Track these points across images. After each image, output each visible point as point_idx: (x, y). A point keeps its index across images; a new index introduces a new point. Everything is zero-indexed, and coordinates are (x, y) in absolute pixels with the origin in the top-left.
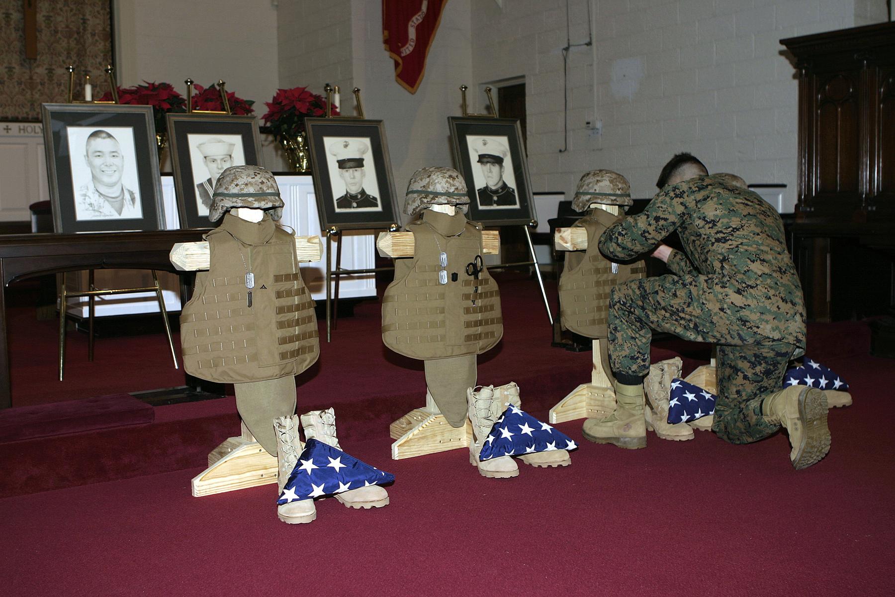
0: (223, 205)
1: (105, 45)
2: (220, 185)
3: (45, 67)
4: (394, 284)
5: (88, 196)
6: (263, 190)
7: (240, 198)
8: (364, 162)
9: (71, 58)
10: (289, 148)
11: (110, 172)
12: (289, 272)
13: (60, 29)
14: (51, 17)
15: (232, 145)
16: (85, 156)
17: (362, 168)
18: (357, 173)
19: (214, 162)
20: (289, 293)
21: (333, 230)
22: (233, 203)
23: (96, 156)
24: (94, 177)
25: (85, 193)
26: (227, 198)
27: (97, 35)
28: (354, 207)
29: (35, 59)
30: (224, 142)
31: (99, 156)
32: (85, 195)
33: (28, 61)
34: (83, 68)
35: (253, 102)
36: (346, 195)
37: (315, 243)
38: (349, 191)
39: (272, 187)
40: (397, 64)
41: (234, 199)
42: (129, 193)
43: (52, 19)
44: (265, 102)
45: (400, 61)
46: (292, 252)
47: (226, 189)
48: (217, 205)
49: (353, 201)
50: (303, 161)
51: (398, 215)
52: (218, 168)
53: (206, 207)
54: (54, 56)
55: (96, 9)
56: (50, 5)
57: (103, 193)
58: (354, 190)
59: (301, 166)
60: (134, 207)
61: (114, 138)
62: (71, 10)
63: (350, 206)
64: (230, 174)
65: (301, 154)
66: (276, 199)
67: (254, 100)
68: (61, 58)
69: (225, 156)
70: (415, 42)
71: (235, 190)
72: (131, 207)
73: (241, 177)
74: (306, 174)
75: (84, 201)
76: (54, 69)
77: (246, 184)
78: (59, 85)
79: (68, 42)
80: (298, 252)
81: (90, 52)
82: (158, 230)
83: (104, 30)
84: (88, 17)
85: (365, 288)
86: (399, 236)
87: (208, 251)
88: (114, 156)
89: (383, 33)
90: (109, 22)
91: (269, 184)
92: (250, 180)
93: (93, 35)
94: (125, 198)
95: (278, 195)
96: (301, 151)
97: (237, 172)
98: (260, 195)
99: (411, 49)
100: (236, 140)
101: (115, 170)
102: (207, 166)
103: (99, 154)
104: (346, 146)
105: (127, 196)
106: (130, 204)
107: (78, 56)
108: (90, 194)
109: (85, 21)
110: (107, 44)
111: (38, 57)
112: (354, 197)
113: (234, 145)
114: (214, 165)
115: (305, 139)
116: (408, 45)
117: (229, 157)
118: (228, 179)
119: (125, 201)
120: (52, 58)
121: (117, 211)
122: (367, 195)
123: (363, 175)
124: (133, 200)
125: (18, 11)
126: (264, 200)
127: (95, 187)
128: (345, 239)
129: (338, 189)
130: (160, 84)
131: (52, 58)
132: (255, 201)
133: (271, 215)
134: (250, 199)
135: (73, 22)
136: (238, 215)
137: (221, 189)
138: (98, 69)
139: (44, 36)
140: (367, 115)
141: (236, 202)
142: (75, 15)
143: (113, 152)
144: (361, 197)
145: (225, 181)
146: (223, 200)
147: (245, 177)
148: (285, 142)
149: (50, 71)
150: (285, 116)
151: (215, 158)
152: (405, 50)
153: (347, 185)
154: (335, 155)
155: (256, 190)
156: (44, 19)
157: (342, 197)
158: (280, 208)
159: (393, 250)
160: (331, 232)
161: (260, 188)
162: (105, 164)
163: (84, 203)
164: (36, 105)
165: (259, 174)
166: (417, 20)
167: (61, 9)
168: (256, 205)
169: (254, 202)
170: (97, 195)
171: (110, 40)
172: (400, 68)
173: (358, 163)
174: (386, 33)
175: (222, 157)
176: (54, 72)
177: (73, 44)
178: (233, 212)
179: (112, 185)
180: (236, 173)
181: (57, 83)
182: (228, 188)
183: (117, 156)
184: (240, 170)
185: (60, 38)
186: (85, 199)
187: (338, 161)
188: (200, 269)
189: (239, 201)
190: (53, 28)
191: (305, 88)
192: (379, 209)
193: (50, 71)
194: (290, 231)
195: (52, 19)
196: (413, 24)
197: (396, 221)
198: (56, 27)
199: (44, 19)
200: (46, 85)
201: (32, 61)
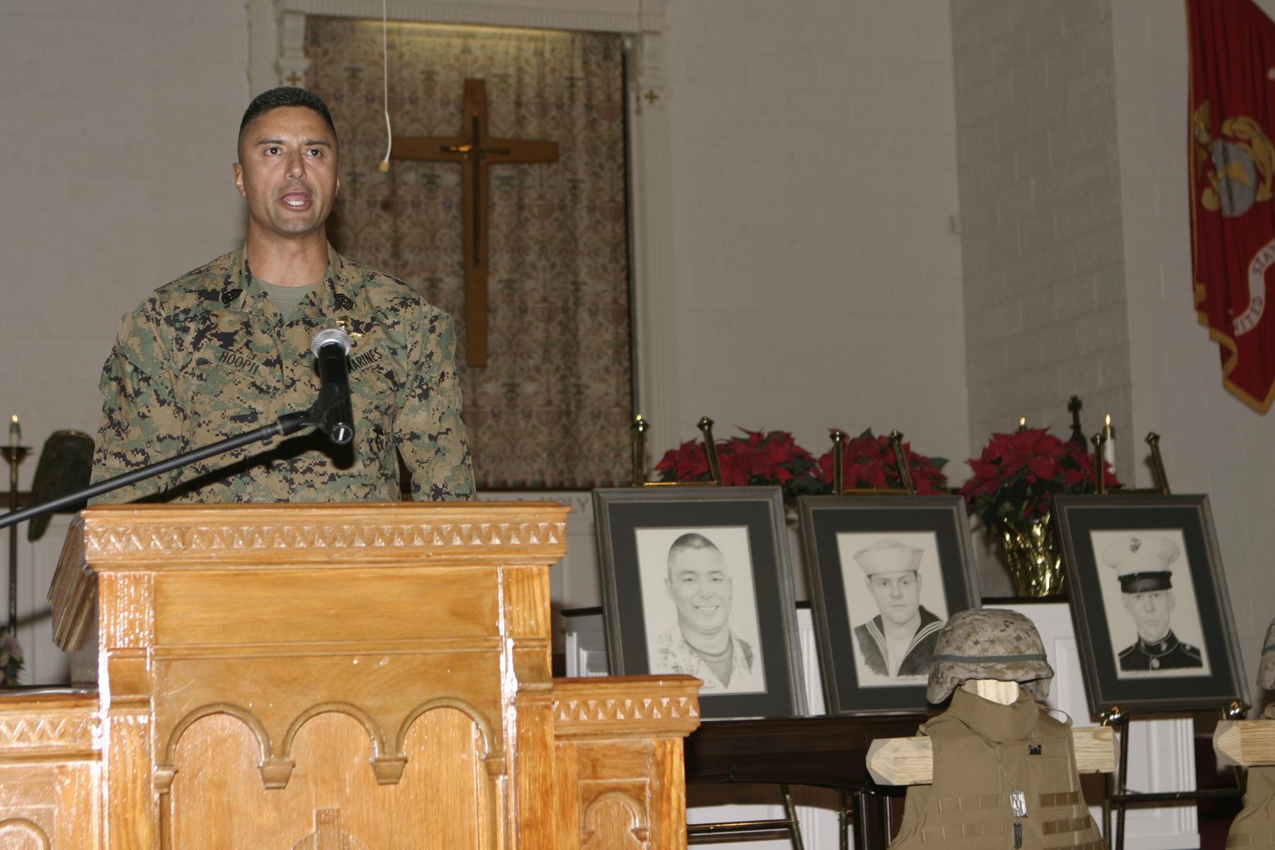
0: (954, 675)
1: (617, 333)
2: (947, 642)
3: (501, 381)
4: (1249, 812)
5: (672, 653)
6: (1020, 651)
7: (982, 665)
8: (1173, 579)
9: (551, 362)
10: (1016, 548)
11: (710, 609)
12: (1063, 790)
13: (530, 305)
14: (515, 281)
15: (918, 552)
16: (665, 581)
17: (1169, 591)
18: (1159, 600)
19: (885, 584)
20: (1064, 826)
21: (1114, 713)
22: (971, 671)
23: (685, 581)
24: (682, 619)
25: (666, 647)
26: (960, 664)
27: (600, 312)
28: (1153, 669)
29: (484, 366)
30: (903, 546)
31: (690, 580)
32: (666, 651)
33: (469, 370)
34: (573, 380)
35: (943, 462)
36: (1138, 644)
37: (1107, 740)
38: (1143, 636)
39: (1035, 644)
40: (1225, 354)
41: (973, 667)
42: (742, 646)
43: (515, 286)
44: (966, 459)
45: (1233, 346)
46: (1068, 755)
47: (958, 648)
48: (942, 676)
49: (1151, 656)
50: (1044, 575)
51: (1243, 683)
52: (893, 597)
53: (873, 670)
54: (518, 359)
55: (601, 261)
56: (513, 259)
57: (698, 647)
58: (1153, 635)
59: (1040, 585)
60: (750, 673)
61: (716, 548)
62: (553, 266)
63: (1145, 666)
64: (964, 624)
65: (1040, 561)
66: (1040, 665)
67: (945, 456)
68: (531, 362)
69: (904, 574)
70: (1263, 305)
71: (974, 652)
72: (745, 672)
73: (983, 629)
74: (1053, 598)
75: (664, 661)
76: (517, 385)
77: (992, 642)
78: (528, 416)
79: (547, 330)
80: (1078, 756)
81: (587, 347)
82: (792, 717)
83: (615, 302)
84: (583, 275)
85: (1176, 833)
86: (1253, 728)
87: (930, 753)
88: (715, 580)
89: (1194, 289)
90: (624, 286)
91: (1030, 640)
92: (997, 633)
93: (594, 313)
94: (734, 655)
95: (1044, 657)
96: (1039, 554)
97: (976, 620)
98: (1016, 660)
99: (1256, 319)
100: (926, 542)
101: (718, 604)
102: (873, 592)
103: (690, 576)
104: (1135, 548)
105: (739, 652)
106: (744, 667)
107: (563, 357)
108: (674, 648)
109: (577, 286)
110: (620, 331)
111: (490, 362)
112: (1154, 649)
113: (922, 551)
114: (885, 591)
115: (1050, 529)
116: (1248, 312)
117: (913, 575)
118: (961, 632)
119: (736, 660)
120: (515, 362)
121: (721, 680)
122: (1180, 644)
123: (1171, 604)
124: (749, 658)
125: (454, 273)
126: (1022, 668)
127: (683, 636)
128: (1135, 727)
129: (1122, 637)
130: (771, 434)
131: (515, 362)
132: (1008, 668)
133: (1031, 691)
134: (1000, 666)
135: (555, 289)
136: (977, 691)
137: (950, 648)
138: (603, 380)
139: (500, 320)
140: (1179, 485)
141: (975, 671)
142: (560, 274)
143: (715, 572)
144: (1168, 649)
145: (955, 636)
146: (953, 667)
147: (990, 630)
148: (1008, 537)
149: (512, 389)
150: (1006, 485)
151: (888, 576)
152: (1242, 322)
153: (1138, 624)
154: (1114, 567)
155: (1009, 650)
156: (500, 286)
157: (1131, 648)
158: (1045, 681)
159: (1244, 753)
160: (1111, 717)
161: (1016, 648)
162: (700, 595)
163: (665, 665)
164: (482, 456)
165: (1012, 623)
166: (1267, 256)
167: (533, 266)
168: (1010, 675)
169: (1006, 671)
170: (687, 649)
171: (626, 321)
172: (1233, 362)
173: (1161, 581)
174: (1202, 289)
175: (899, 575)
176: (518, 390)
177: (555, 333)
178: (967, 687)
179: (710, 633)
180: (975, 623)
181: (523, 411)
182: (961, 648)
183: (721, 580)
184: (979, 618)
185: (530, 323)
186: (666, 658)
187: (1121, 579)
188: (917, 783)
189: (980, 669)
190: (518, 304)
191: (1046, 430)
192: (1205, 670)
193: (512, 389)
194: (1062, 719)
195: (515, 286)
196: (1257, 266)
197: (1239, 696)
198: (523, 302)
199: (500, 286)
200: (504, 417)
201: (477, 370)
